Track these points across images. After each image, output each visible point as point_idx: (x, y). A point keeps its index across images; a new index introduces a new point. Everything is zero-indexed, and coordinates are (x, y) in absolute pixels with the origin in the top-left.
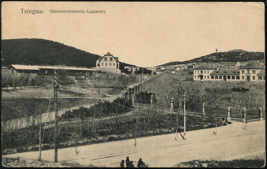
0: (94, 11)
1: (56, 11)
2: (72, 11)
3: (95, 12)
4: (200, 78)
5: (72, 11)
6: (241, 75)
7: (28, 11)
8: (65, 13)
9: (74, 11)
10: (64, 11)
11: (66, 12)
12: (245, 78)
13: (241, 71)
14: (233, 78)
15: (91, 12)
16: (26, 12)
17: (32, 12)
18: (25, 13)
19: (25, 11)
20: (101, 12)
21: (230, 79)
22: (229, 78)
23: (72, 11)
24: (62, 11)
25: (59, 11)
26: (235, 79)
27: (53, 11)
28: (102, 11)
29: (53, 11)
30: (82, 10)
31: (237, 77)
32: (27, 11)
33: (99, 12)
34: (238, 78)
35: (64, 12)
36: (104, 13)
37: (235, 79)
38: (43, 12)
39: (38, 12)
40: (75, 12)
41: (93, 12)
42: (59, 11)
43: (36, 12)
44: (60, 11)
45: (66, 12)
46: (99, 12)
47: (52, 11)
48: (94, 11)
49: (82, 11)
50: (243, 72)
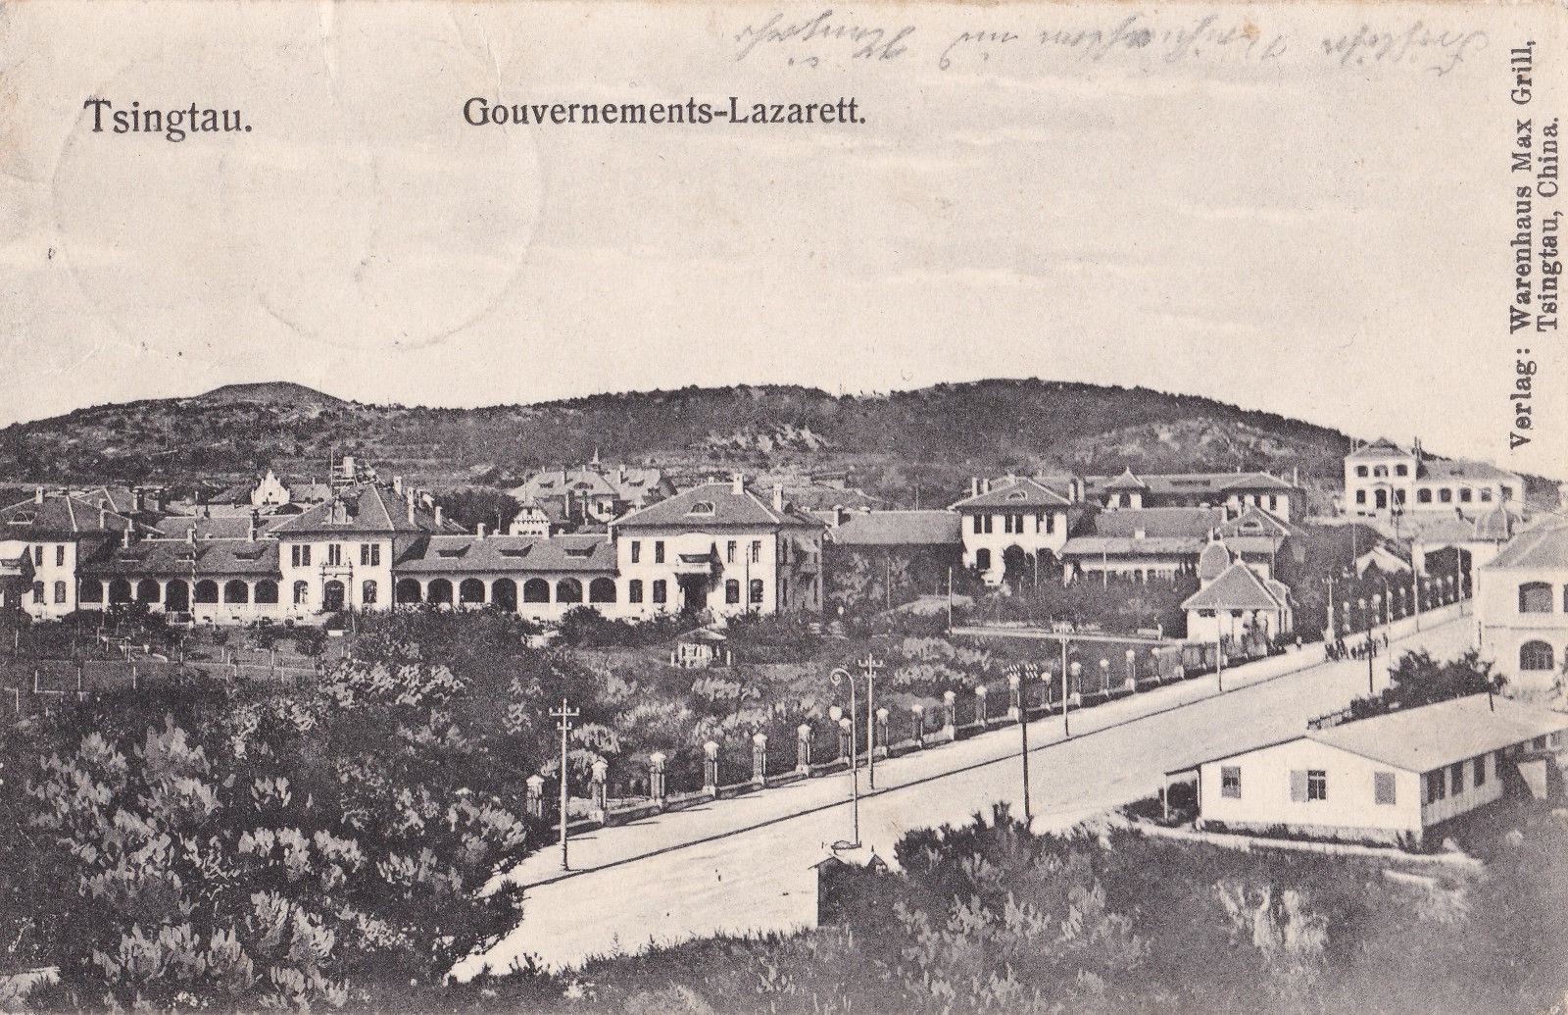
0: (781, 107)
1: (600, 117)
2: (629, 112)
3: (785, 113)
4: (1394, 570)
5: (629, 112)
6: (290, 574)
7: (136, 113)
8: (572, 120)
9: (638, 112)
10: (566, 107)
11: (579, 114)
12: (315, 596)
13: (630, 545)
14: (237, 594)
15: (760, 114)
16: (122, 127)
17: (164, 123)
18: (116, 129)
19: (121, 116)
20: (559, 117)
21: (216, 601)
22: (207, 594)
23: (671, 107)
24: (548, 111)
25: (530, 111)
26: (546, 599)
27: (485, 111)
28: (837, 110)
29: (485, 111)
30: (698, 102)
31: (229, 589)
32: (130, 119)
33: (815, 113)
34: (267, 594)
35: (567, 115)
36: (853, 120)
37: (546, 599)
38: (242, 126)
39: (795, 117)
40: (600, 117)
41: (769, 115)
42: (530, 111)
43: (198, 125)
44: (540, 110)
45: (579, 114)
46: (815, 113)
47: (476, 114)
48: (781, 107)
49: (696, 111)
50: (301, 557)
